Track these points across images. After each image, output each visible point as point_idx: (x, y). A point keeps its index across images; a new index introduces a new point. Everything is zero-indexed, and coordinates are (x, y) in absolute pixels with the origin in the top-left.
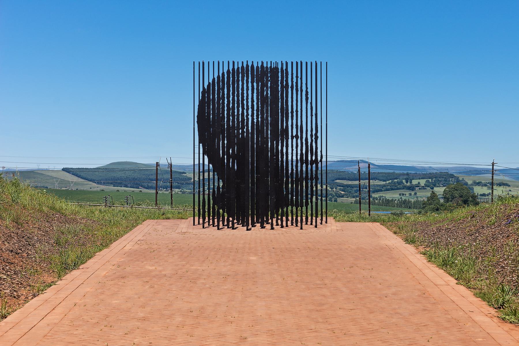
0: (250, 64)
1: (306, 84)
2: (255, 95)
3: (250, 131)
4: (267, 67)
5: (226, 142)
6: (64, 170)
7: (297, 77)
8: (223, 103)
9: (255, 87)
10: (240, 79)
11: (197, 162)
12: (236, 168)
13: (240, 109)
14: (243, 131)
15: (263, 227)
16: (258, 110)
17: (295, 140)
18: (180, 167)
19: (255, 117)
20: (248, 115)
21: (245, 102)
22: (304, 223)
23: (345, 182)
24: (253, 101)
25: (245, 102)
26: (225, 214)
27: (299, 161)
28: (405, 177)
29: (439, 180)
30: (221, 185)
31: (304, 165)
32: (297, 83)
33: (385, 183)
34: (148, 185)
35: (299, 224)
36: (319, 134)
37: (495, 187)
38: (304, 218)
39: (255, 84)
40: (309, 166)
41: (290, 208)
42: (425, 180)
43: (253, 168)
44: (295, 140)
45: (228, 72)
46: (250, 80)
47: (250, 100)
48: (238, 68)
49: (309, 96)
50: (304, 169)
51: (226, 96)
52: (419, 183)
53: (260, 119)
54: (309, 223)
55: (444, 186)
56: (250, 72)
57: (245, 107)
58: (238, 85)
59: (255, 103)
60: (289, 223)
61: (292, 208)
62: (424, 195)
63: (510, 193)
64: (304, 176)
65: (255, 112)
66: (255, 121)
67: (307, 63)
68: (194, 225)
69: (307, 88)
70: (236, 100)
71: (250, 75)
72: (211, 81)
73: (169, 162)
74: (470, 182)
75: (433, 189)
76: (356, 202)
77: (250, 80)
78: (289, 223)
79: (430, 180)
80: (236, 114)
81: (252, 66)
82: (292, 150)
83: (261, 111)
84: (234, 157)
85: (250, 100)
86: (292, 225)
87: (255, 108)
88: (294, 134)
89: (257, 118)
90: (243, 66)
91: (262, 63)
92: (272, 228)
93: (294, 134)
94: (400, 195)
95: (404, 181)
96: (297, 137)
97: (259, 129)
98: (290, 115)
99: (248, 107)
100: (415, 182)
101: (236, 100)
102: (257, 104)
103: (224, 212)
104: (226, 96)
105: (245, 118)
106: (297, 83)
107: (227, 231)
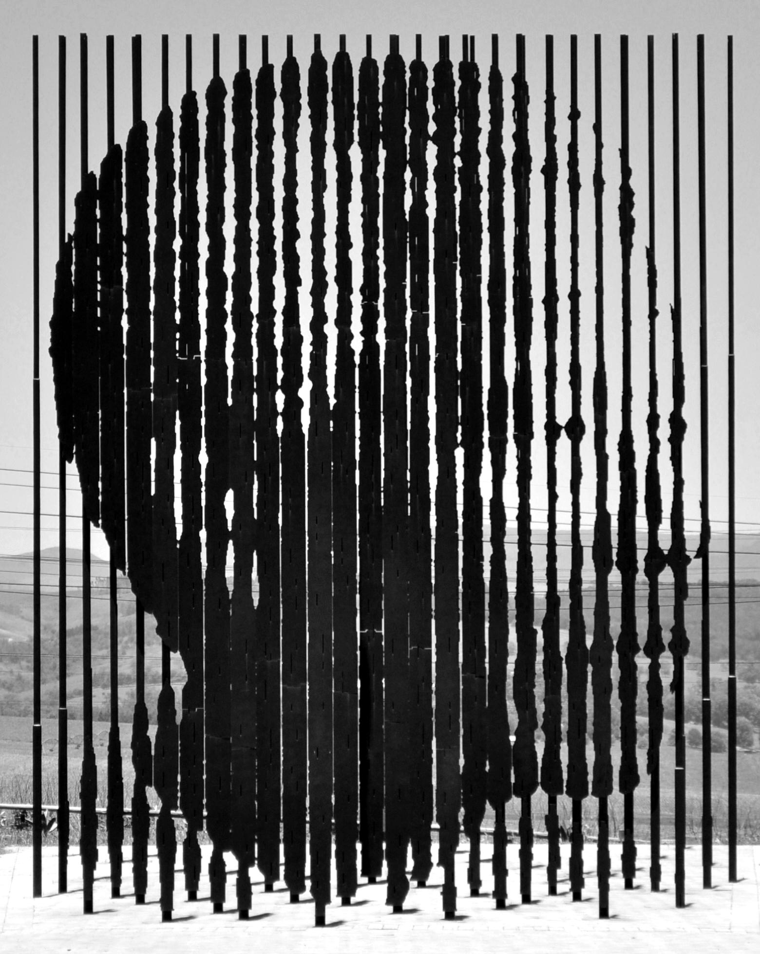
0: (330, 54)
1: (624, 153)
2: (356, 208)
4: (418, 66)
5: (203, 459)
8: (190, 253)
9: (357, 168)
10: (278, 124)
11: (50, 541)
13: (279, 281)
14: (293, 403)
15: (396, 899)
16: (369, 290)
19: (356, 327)
20: (319, 319)
22: (616, 882)
31: (615, 577)
32: (573, 148)
36: (691, 413)
38: (616, 851)
39: (355, 154)
40: (641, 577)
41: (539, 798)
44: (564, 443)
45: (216, 90)
47: (330, 242)
48: (267, 70)
49: (640, 213)
51: (202, 217)
53: (381, 339)
54: (642, 878)
58: (266, 156)
59: (356, 255)
60: (539, 878)
61: (552, 802)
64: (615, 627)
65: (356, 299)
66: (357, 344)
67: (520, 40)
68: (37, 892)
69: (626, 172)
70: (255, 235)
71: (330, 109)
72: (122, 139)
77: (330, 136)
78: (539, 878)
81: (342, 58)
82: (553, 497)
84: (253, 534)
85: (330, 242)
86: (553, 891)
88: (563, 416)
89: (369, 331)
91: (394, 41)
92: (450, 913)
93: (563, 416)
97: (361, 374)
98: (538, 313)
101: (255, 235)
102: (369, 255)
104: (202, 217)
106: (573, 148)
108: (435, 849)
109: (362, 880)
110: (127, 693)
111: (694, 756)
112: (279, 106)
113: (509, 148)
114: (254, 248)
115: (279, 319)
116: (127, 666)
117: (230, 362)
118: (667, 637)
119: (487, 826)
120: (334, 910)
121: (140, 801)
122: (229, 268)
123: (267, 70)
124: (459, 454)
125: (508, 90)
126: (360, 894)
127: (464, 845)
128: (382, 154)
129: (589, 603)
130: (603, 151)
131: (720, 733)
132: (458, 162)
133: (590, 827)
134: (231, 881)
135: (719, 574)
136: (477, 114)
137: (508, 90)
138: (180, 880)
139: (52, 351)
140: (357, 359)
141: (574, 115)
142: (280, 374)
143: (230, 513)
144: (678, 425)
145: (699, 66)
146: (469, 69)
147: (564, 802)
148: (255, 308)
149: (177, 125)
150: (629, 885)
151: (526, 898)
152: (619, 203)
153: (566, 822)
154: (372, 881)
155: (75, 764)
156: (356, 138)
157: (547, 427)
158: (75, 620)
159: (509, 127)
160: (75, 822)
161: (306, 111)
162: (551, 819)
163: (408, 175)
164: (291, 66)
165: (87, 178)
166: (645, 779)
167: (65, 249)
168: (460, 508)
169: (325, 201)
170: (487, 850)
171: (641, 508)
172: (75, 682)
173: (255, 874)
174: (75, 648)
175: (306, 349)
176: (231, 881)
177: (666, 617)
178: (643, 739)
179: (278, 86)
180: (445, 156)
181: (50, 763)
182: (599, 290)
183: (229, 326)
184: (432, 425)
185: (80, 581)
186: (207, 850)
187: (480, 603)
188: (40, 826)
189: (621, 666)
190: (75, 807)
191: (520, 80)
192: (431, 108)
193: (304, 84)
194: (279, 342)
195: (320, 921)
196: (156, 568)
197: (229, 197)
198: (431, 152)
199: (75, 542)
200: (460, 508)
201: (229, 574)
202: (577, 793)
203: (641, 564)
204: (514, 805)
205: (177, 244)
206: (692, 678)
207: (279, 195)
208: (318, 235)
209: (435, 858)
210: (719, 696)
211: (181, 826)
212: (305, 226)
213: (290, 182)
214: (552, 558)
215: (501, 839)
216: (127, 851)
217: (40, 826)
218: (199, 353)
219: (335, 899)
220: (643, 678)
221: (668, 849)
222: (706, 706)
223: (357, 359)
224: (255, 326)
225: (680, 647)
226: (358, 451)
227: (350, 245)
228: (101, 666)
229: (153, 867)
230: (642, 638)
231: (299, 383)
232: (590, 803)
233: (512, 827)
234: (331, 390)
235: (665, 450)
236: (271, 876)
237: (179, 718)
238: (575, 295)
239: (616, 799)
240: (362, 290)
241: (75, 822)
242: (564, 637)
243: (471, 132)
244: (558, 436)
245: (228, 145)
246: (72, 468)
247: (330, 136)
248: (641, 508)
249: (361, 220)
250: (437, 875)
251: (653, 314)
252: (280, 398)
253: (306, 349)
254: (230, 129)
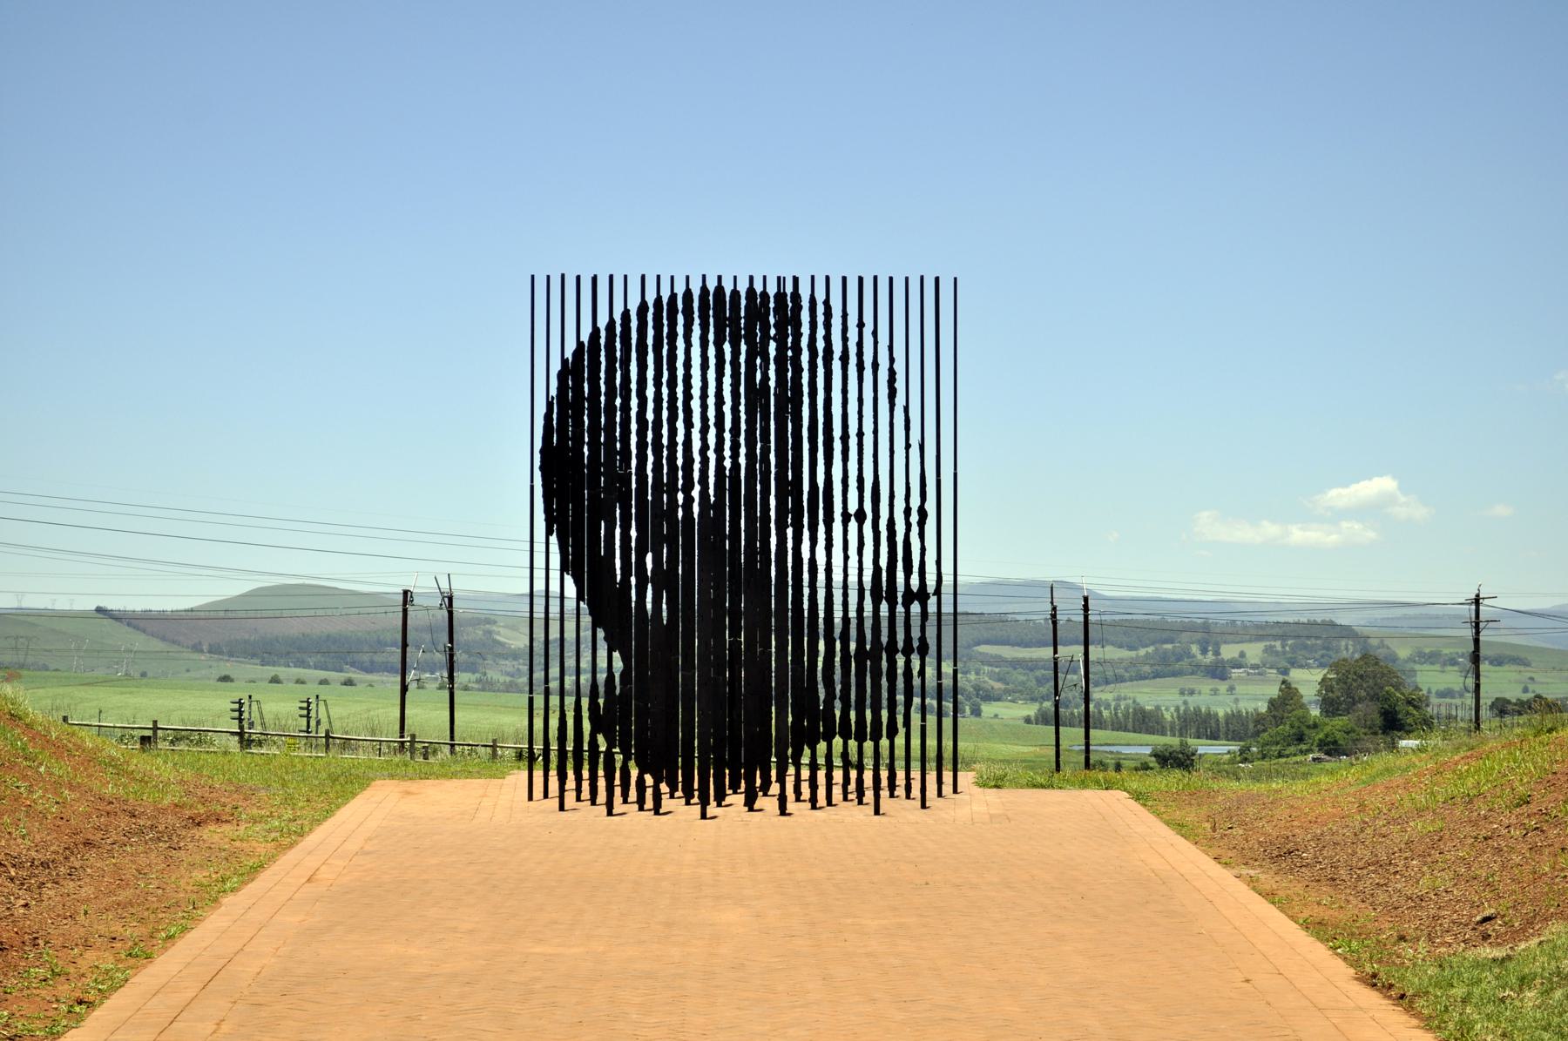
2: (727, 380)
4: (765, 294)
6: (99, 610)
8: (626, 408)
9: (728, 357)
10: (680, 329)
11: (539, 586)
13: (680, 425)
14: (689, 500)
15: (750, 803)
17: (853, 525)
18: (477, 597)
19: (727, 453)
22: (885, 793)
23: (1008, 652)
26: (632, 763)
27: (867, 594)
28: (1199, 636)
29: (1305, 647)
31: (884, 607)
32: (860, 345)
33: (1133, 654)
34: (372, 662)
35: (869, 795)
37: (1484, 667)
38: (884, 774)
39: (727, 347)
40: (900, 609)
41: (838, 741)
42: (1261, 646)
43: (715, 603)
44: (853, 525)
45: (643, 308)
47: (711, 401)
48: (673, 297)
49: (900, 385)
51: (634, 386)
52: (1242, 655)
53: (742, 460)
54: (900, 791)
55: (1322, 665)
59: (727, 409)
60: (837, 791)
62: (1255, 697)
63: (1531, 687)
64: (884, 639)
65: (727, 436)
66: (727, 463)
68: (530, 798)
69: (892, 360)
72: (585, 338)
73: (445, 586)
74: (1403, 653)
75: (1285, 672)
76: (1042, 719)
77: (711, 337)
78: (837, 791)
79: (1278, 644)
82: (846, 558)
84: (664, 579)
85: (711, 401)
86: (845, 799)
87: (728, 424)
92: (783, 811)
93: (853, 507)
94: (1182, 693)
95: (1195, 649)
99: (696, 414)
100: (1229, 652)
102: (735, 410)
103: (610, 746)
104: (634, 386)
106: (860, 345)
107: (632, 818)
108: (774, 773)
109: (729, 792)
110: (585, 678)
111: (932, 719)
112: (680, 319)
113: (820, 345)
114: (665, 405)
115: (680, 448)
116: (585, 663)
117: (650, 474)
118: (916, 644)
119: (805, 760)
120: (712, 809)
121: (593, 743)
122: (650, 416)
123: (673, 297)
124: (790, 531)
125: (820, 309)
126: (728, 800)
127: (791, 770)
128: (743, 348)
129: (868, 624)
131: (948, 705)
132: (790, 353)
133: (869, 762)
134: (649, 792)
135: (947, 608)
136: (800, 324)
137: (820, 309)
138: (618, 791)
141: (861, 325)
142: (680, 482)
143: (649, 566)
144: (923, 513)
145: (936, 294)
146: (796, 296)
147: (853, 744)
148: (665, 441)
149: (618, 329)
150: (892, 796)
151: (830, 803)
153: (854, 757)
154: (735, 792)
155: (554, 723)
158: (554, 634)
159: (821, 332)
160: (554, 756)
161: (697, 321)
162: (845, 754)
163: (758, 361)
164: (688, 294)
165: (564, 361)
166: (902, 731)
167: (549, 405)
168: (790, 565)
170: (805, 773)
171: (900, 565)
172: (554, 671)
173: (664, 788)
174: (554, 651)
175: (697, 466)
176: (649, 792)
177: (916, 633)
178: (900, 709)
179: (680, 306)
180: (781, 349)
181: (538, 723)
182: (875, 432)
183: (649, 452)
184: (773, 514)
185: (558, 609)
186: (634, 773)
187: (801, 624)
188: (532, 759)
190: (554, 746)
191: (827, 303)
192: (772, 320)
193: (696, 305)
194: (680, 462)
195: (704, 816)
196: (604, 601)
197: (650, 373)
198: (772, 346)
199: (555, 587)
200: (790, 565)
201: (649, 606)
202: (861, 739)
203: (900, 600)
204: (822, 747)
205: (618, 402)
206: (930, 672)
207: (680, 372)
208: (704, 397)
209: (774, 778)
210: (947, 682)
211: (619, 758)
212: (696, 392)
213: (688, 365)
214: (845, 595)
215: (814, 767)
216: (586, 774)
217: (532, 759)
219: (713, 803)
221: (916, 774)
222: (940, 686)
224: (665, 453)
225: (923, 650)
228: (570, 663)
229: (602, 783)
230: (900, 645)
231: (692, 488)
232: (868, 745)
233: (821, 761)
234: (711, 492)
235: (915, 530)
237: (618, 691)
238: (860, 434)
239: (884, 742)
241: (554, 756)
242: (853, 646)
243: (798, 336)
245: (650, 341)
246: (554, 539)
247: (711, 337)
248: (900, 565)
250: (775, 788)
251: (908, 446)
252: (680, 496)
253: (697, 466)
254: (651, 332)
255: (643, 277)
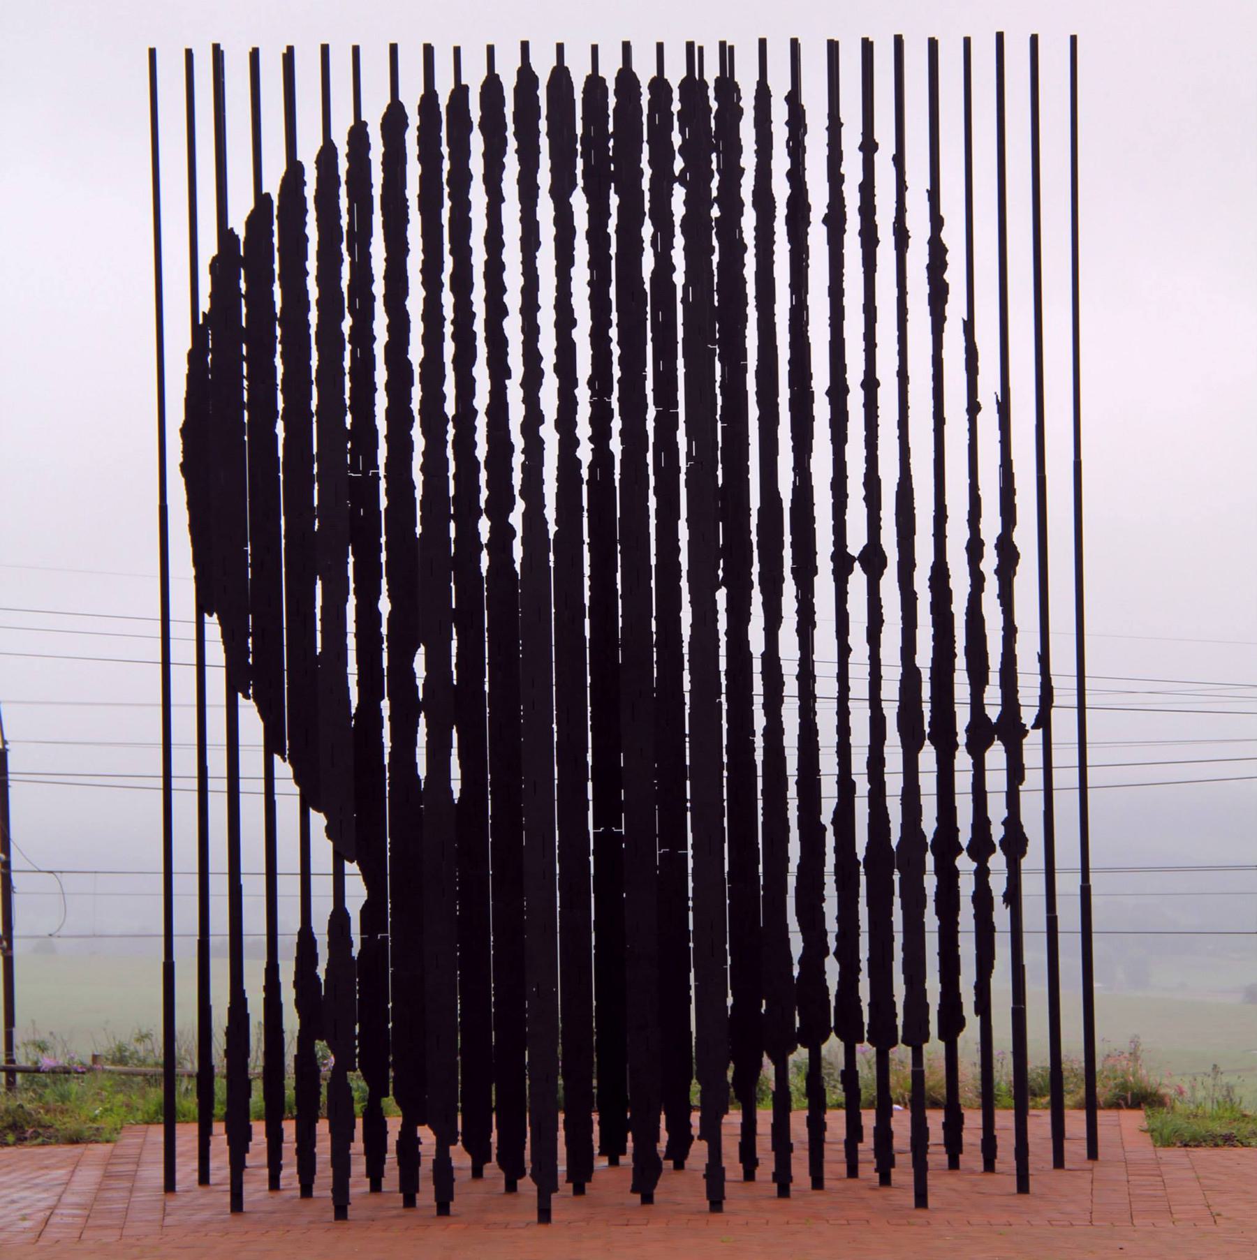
0: (543, 68)
3: (552, 529)
5: (385, 606)
7: (869, 147)
8: (363, 335)
9: (581, 221)
10: (477, 165)
12: (456, 786)
13: (481, 372)
17: (858, 580)
19: (584, 430)
20: (534, 418)
21: (513, 327)
22: (937, 1155)
24: (565, 320)
25: (513, 327)
26: (389, 1102)
30: (357, 892)
31: (928, 757)
32: (867, 188)
35: (903, 1173)
39: (579, 202)
41: (833, 1047)
44: (858, 580)
46: (544, 178)
47: (547, 317)
48: (460, 92)
49: (954, 275)
50: (928, 783)
51: (379, 288)
53: (616, 445)
54: (972, 1156)
56: (543, 125)
57: (515, 360)
59: (581, 335)
64: (929, 825)
65: (583, 394)
66: (585, 453)
68: (170, 1184)
69: (937, 222)
71: (544, 142)
72: (272, 186)
77: (544, 178)
80: (450, 408)
81: (560, 75)
82: (844, 651)
83: (618, 388)
84: (452, 705)
85: (547, 317)
87: (584, 368)
88: (856, 542)
90: (492, 85)
93: (856, 542)
96: (873, 559)
97: (608, 507)
103: (377, 1092)
104: (379, 288)
105: (518, 441)
106: (867, 188)
109: (601, 1163)
130: (908, 194)
139: (184, 467)
140: (585, 473)
147: (866, 1052)
152: (927, 262)
156: (580, 182)
157: (834, 557)
169: (539, 263)
180: (697, 202)
189: (938, 871)
218: (377, 468)
220: (967, 886)
223: (585, 473)
226: (587, 594)
227: (573, 323)
230: (965, 837)
235: (992, 585)
236: (480, 1157)
240: (590, 383)
244: (851, 570)
249: (588, 290)
250: (699, 1151)
255: (189, 54)
